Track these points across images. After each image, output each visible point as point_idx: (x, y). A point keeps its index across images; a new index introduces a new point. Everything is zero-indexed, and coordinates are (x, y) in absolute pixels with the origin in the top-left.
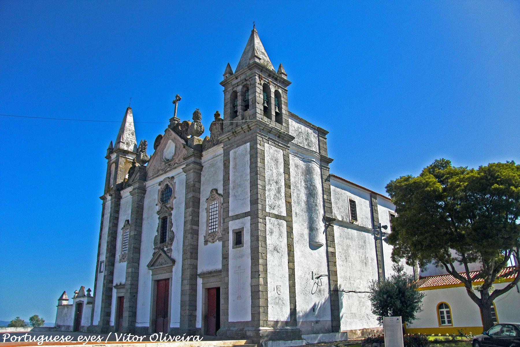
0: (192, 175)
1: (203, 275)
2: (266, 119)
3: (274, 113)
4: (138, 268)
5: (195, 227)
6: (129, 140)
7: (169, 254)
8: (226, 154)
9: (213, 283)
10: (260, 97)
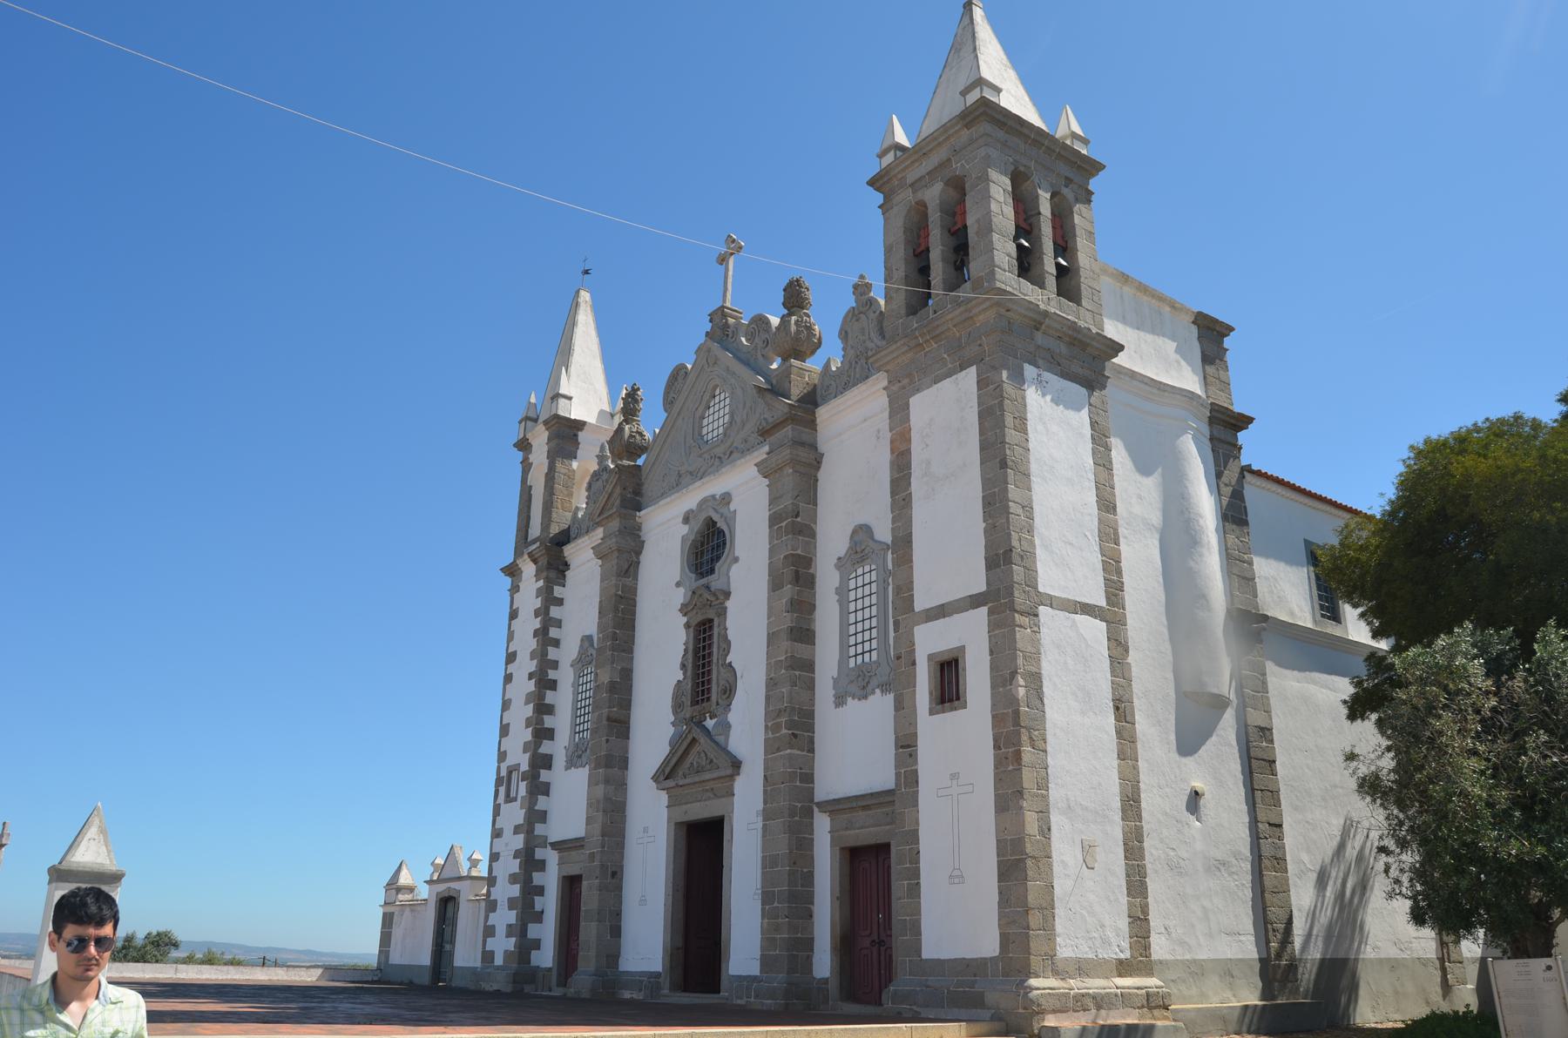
0: (788, 477)
1: (838, 807)
2: (1027, 291)
3: (1050, 268)
4: (621, 785)
5: (801, 650)
6: (587, 395)
7: (720, 739)
8: (899, 411)
9: (865, 833)
10: (1002, 212)
